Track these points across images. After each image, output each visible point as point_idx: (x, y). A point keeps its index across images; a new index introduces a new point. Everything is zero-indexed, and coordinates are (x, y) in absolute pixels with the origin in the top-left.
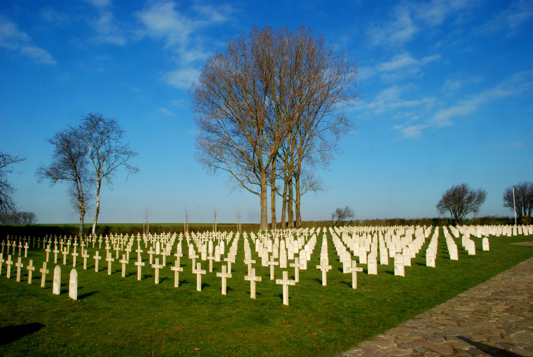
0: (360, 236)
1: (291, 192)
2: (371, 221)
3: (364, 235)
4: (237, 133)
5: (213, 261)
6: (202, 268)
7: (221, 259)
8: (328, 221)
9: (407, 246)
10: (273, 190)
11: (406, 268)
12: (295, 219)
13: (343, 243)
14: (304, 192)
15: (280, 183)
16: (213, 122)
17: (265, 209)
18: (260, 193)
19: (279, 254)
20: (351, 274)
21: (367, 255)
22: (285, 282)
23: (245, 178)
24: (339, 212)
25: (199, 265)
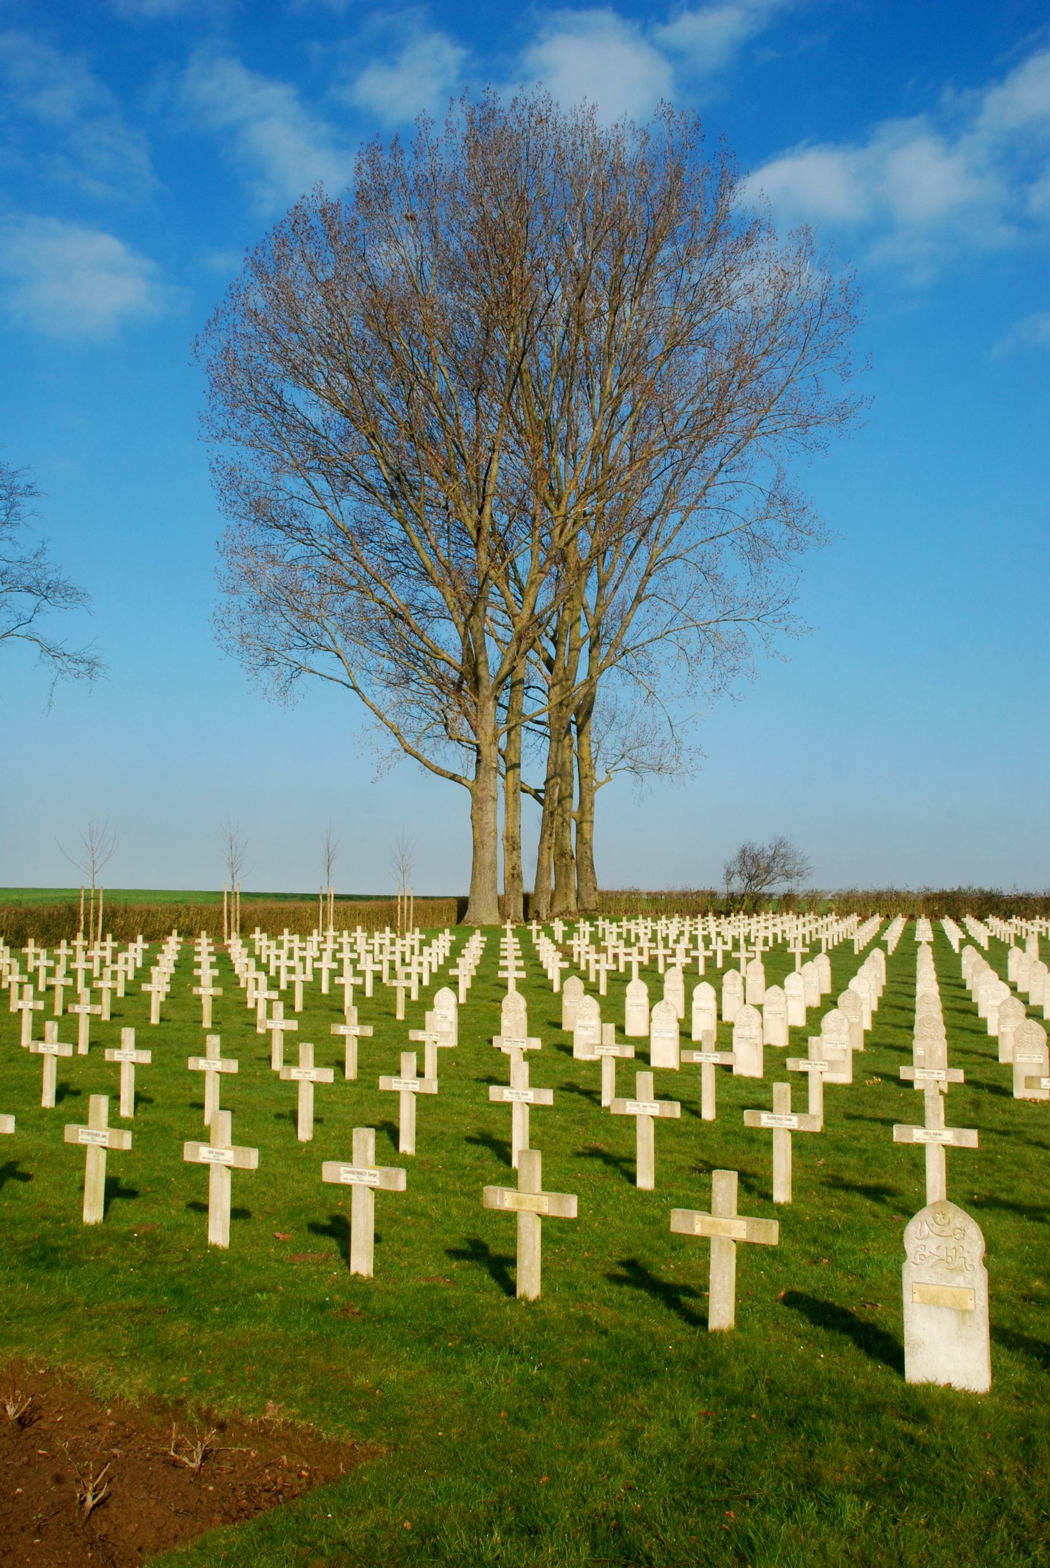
6: (320, 1061)
8: (698, 893)
13: (1014, 988)
17: (489, 841)
18: (471, 776)
20: (596, 1066)
22: (780, 1122)
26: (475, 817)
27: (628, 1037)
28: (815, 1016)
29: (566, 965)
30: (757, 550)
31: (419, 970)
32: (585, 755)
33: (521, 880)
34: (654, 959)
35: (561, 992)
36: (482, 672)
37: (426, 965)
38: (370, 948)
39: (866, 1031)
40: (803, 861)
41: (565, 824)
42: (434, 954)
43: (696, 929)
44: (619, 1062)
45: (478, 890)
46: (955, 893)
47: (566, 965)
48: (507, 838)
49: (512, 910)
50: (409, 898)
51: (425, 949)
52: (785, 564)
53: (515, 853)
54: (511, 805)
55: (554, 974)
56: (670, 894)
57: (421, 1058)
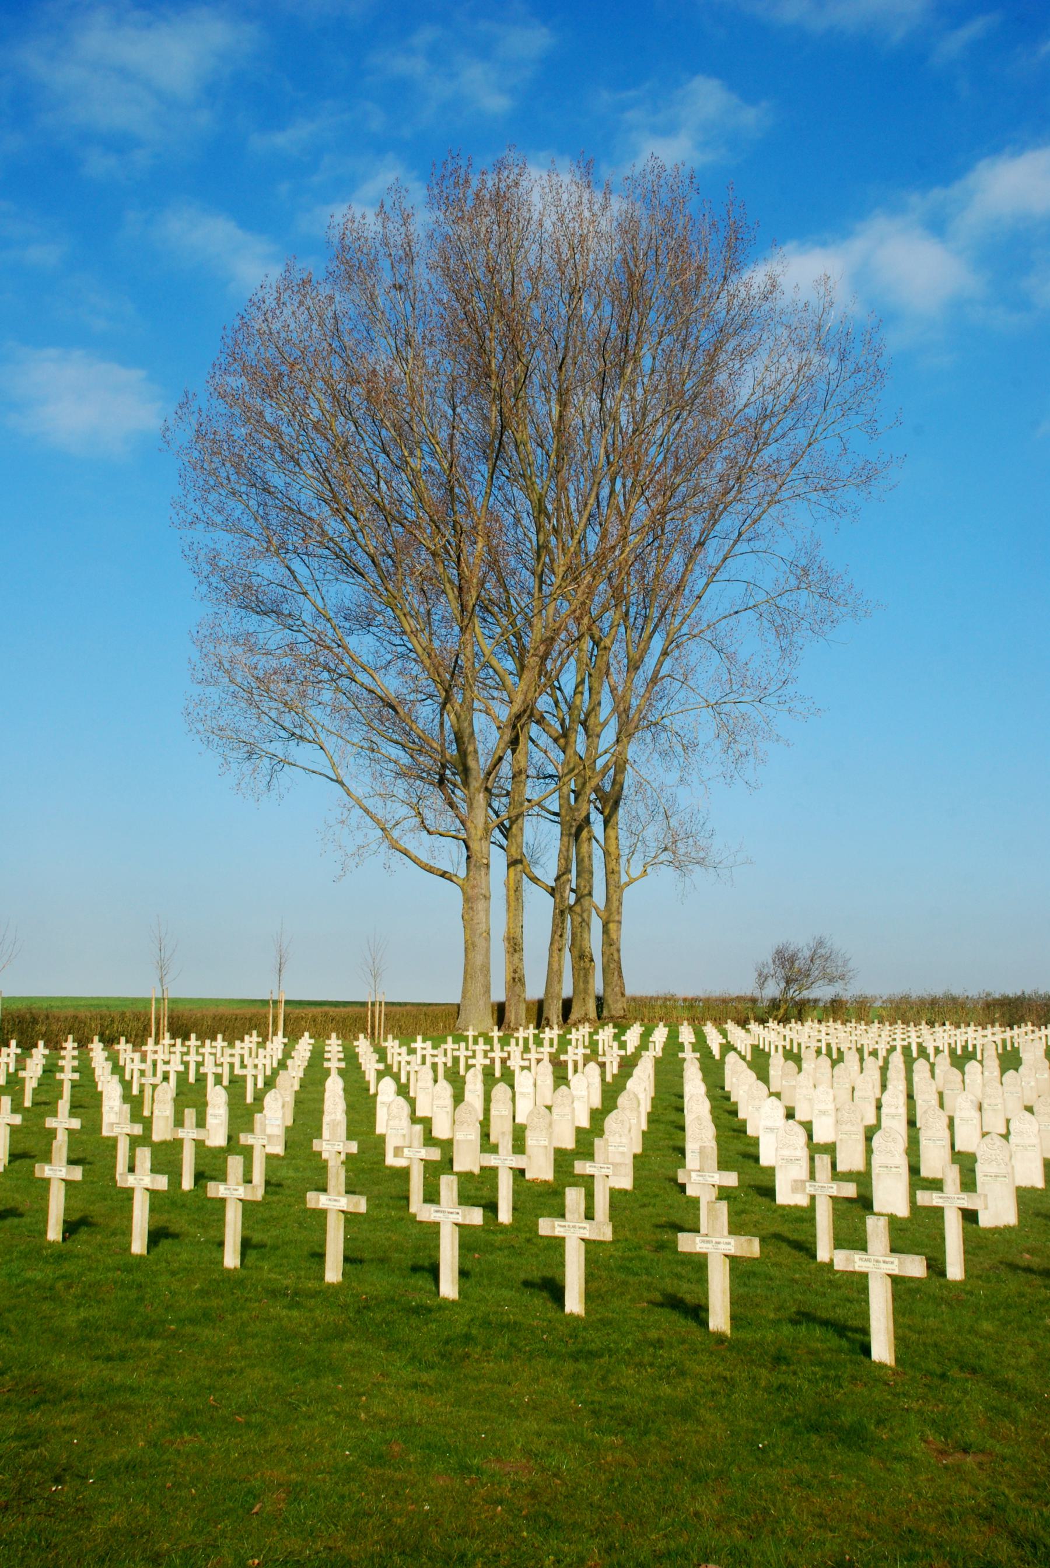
0: (834, 1063)
1: (585, 872)
2: (922, 1001)
3: (851, 1058)
4: (366, 622)
5: (199, 1144)
7: (230, 1138)
8: (739, 999)
9: (1029, 1109)
10: (513, 863)
11: (1024, 1197)
12: (597, 985)
14: (636, 870)
15: (542, 837)
16: (268, 570)
17: (480, 942)
18: (462, 873)
19: (869, 1151)
21: (869, 1139)
23: (404, 811)
24: (785, 959)
25: (144, 1156)
26: (466, 917)
27: (925, 1180)
28: (598, 1116)
29: (381, 1066)
30: (782, 625)
31: (254, 1072)
32: (612, 849)
33: (523, 985)
34: (456, 1060)
35: (376, 1095)
36: (471, 763)
37: (260, 1066)
38: (526, 1063)
39: (643, 1132)
40: (846, 962)
41: (585, 924)
42: (268, 1057)
43: (894, 1040)
44: (428, 1164)
45: (468, 995)
46: (1019, 998)
47: (381, 1066)
48: (508, 939)
49: (513, 1017)
50: (380, 1003)
51: (261, 1051)
52: (820, 639)
53: (517, 955)
54: (513, 904)
55: (371, 1076)
56: (708, 1000)
57: (590, 1196)
